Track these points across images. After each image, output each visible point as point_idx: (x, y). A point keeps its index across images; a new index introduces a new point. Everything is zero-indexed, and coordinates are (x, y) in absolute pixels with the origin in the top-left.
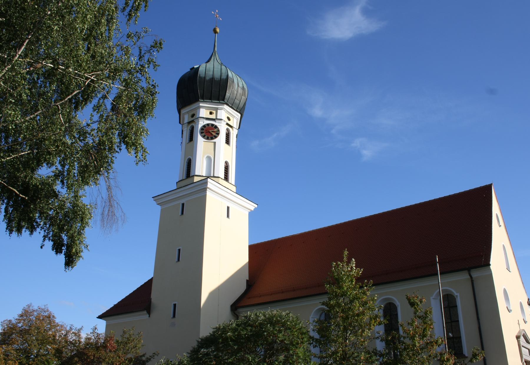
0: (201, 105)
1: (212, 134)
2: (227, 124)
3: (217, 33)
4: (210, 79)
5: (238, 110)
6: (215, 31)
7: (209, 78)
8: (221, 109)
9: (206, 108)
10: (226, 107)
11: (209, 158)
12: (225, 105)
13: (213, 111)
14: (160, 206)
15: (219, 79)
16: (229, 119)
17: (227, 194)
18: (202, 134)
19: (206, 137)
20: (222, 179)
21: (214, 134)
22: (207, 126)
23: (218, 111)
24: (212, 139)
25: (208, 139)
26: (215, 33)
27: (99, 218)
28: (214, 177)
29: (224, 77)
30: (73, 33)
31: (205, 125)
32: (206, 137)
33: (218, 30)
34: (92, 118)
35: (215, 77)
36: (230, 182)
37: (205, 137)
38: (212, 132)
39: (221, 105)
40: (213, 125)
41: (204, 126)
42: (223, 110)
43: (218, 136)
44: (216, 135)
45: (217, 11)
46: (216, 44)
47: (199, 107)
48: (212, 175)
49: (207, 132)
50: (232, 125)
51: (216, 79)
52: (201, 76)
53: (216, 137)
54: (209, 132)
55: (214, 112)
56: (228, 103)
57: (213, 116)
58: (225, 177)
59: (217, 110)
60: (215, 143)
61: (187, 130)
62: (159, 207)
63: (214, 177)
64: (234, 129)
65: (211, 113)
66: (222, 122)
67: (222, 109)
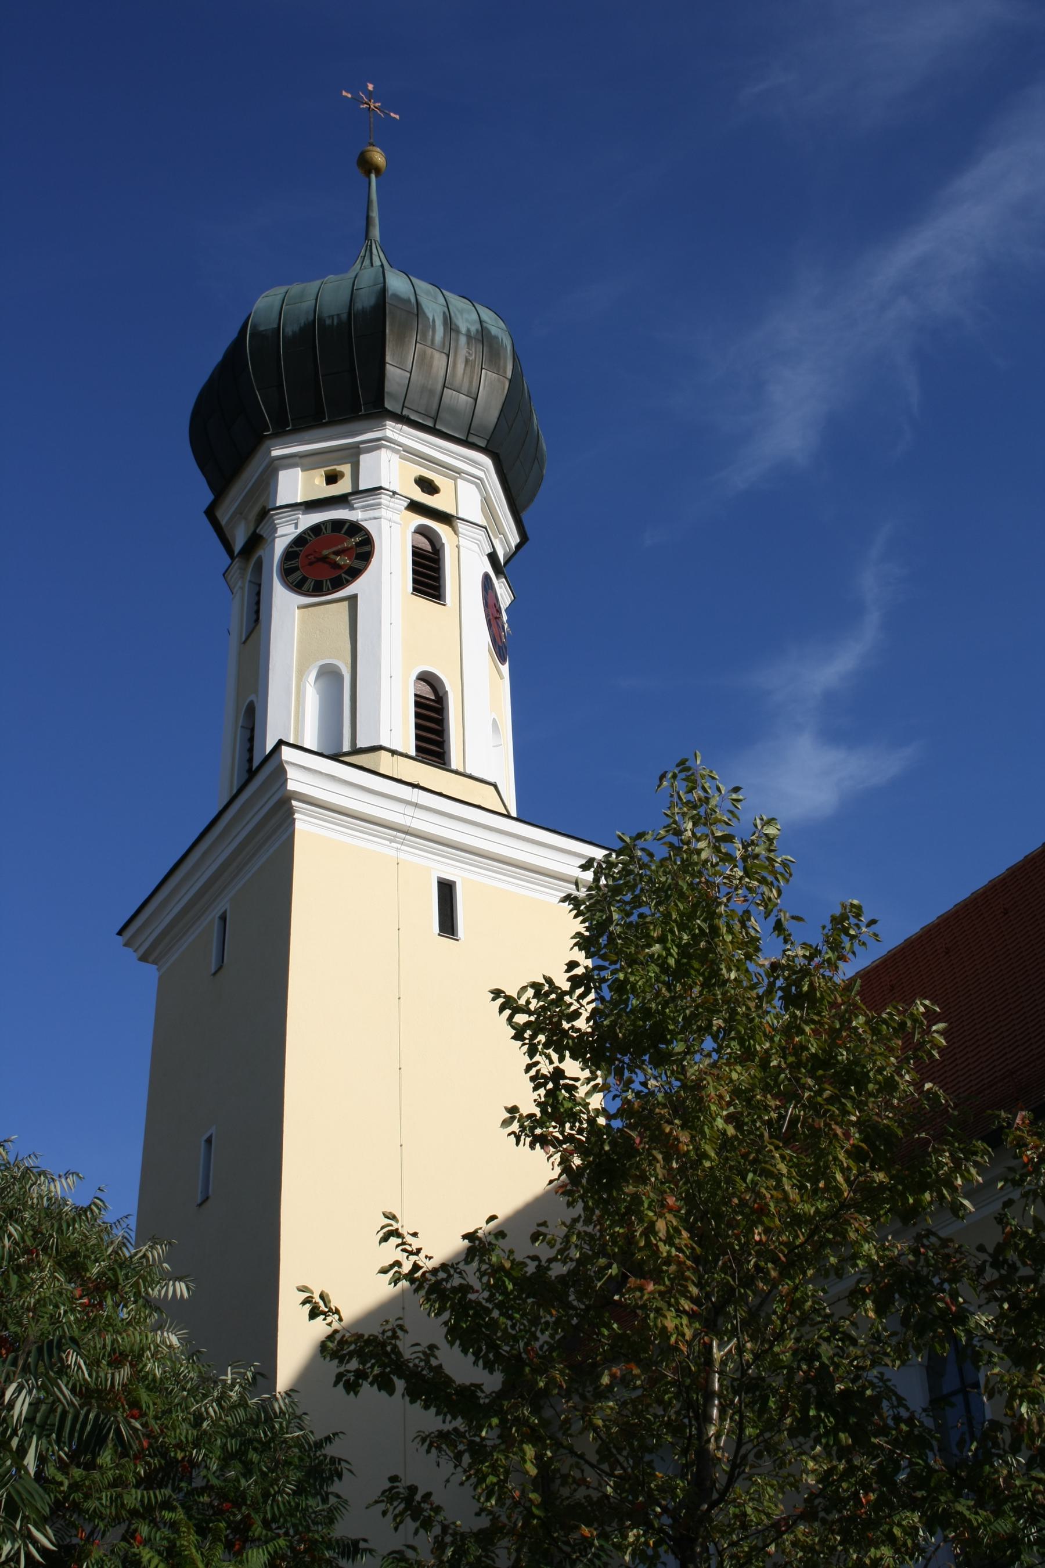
0: (275, 453)
1: (336, 566)
2: (415, 507)
3: (378, 171)
4: (302, 330)
5: (472, 439)
6: (367, 166)
7: (296, 328)
8: (375, 445)
9: (305, 461)
10: (392, 430)
11: (329, 675)
12: (390, 424)
13: (339, 468)
14: (154, 963)
15: (344, 317)
16: (428, 486)
17: (419, 813)
18: (291, 578)
19: (309, 584)
20: (394, 752)
21: (344, 561)
22: (312, 539)
23: (363, 458)
24: (339, 584)
25: (317, 590)
26: (368, 174)
27: (447, 1427)
28: (356, 751)
29: (366, 300)
30: (891, 1050)
31: (304, 532)
32: (309, 584)
33: (379, 158)
34: (833, 1276)
35: (325, 315)
36: (454, 767)
37: (305, 587)
38: (337, 553)
39: (371, 430)
40: (337, 525)
41: (300, 541)
42: (383, 450)
43: (365, 568)
44: (357, 564)
45: (371, 87)
46: (375, 214)
47: (273, 468)
48: (346, 747)
49: (311, 564)
50: (450, 510)
51: (328, 322)
52: (262, 328)
53: (355, 573)
54: (325, 559)
55: (346, 469)
56: (406, 412)
57: (343, 487)
58: (418, 749)
59: (353, 455)
60: (353, 600)
61: (242, 588)
62: (150, 973)
63: (356, 751)
64: (461, 526)
65: (332, 479)
66: (384, 499)
67: (378, 448)
